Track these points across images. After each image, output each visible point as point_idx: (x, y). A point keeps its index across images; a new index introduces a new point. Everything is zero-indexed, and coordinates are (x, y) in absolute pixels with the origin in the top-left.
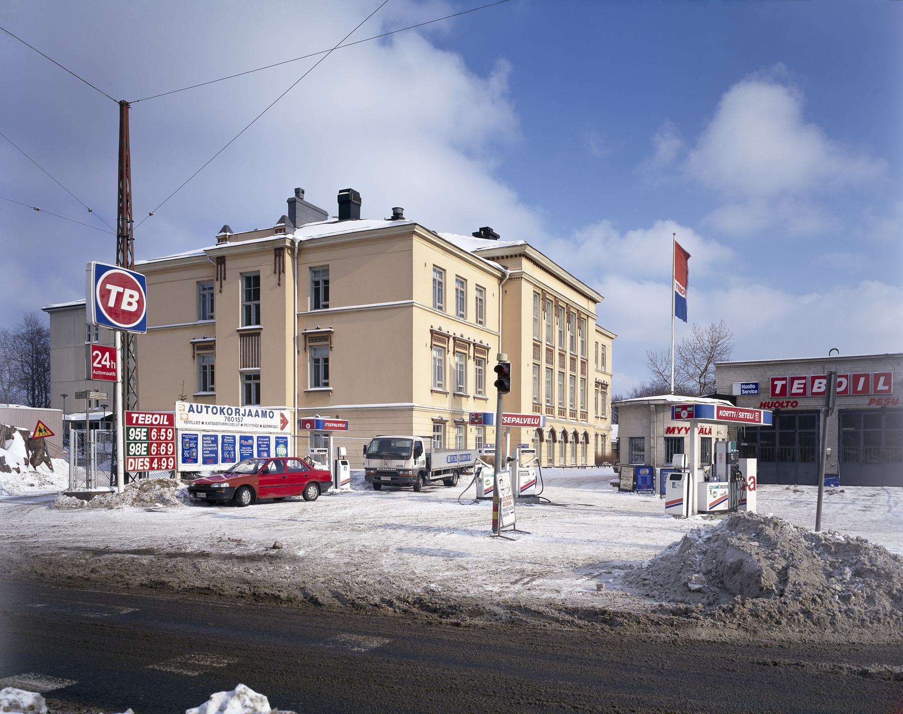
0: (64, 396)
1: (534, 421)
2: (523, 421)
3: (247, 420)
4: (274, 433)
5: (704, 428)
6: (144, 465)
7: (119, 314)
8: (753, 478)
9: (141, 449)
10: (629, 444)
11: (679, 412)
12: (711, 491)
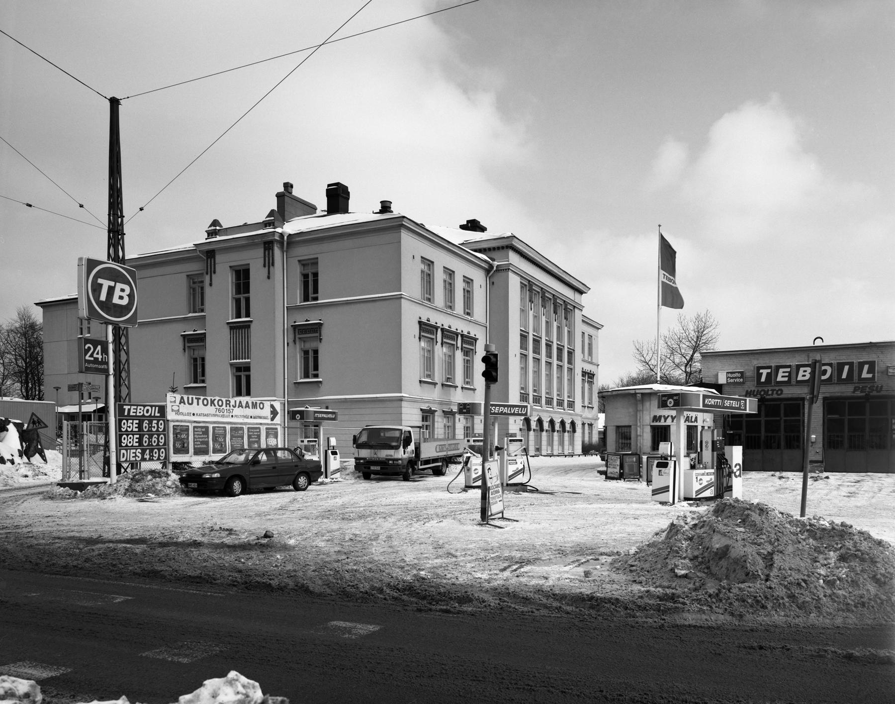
1: (521, 411)
2: (510, 411)
3: (237, 411)
6: (136, 456)
9: (133, 440)
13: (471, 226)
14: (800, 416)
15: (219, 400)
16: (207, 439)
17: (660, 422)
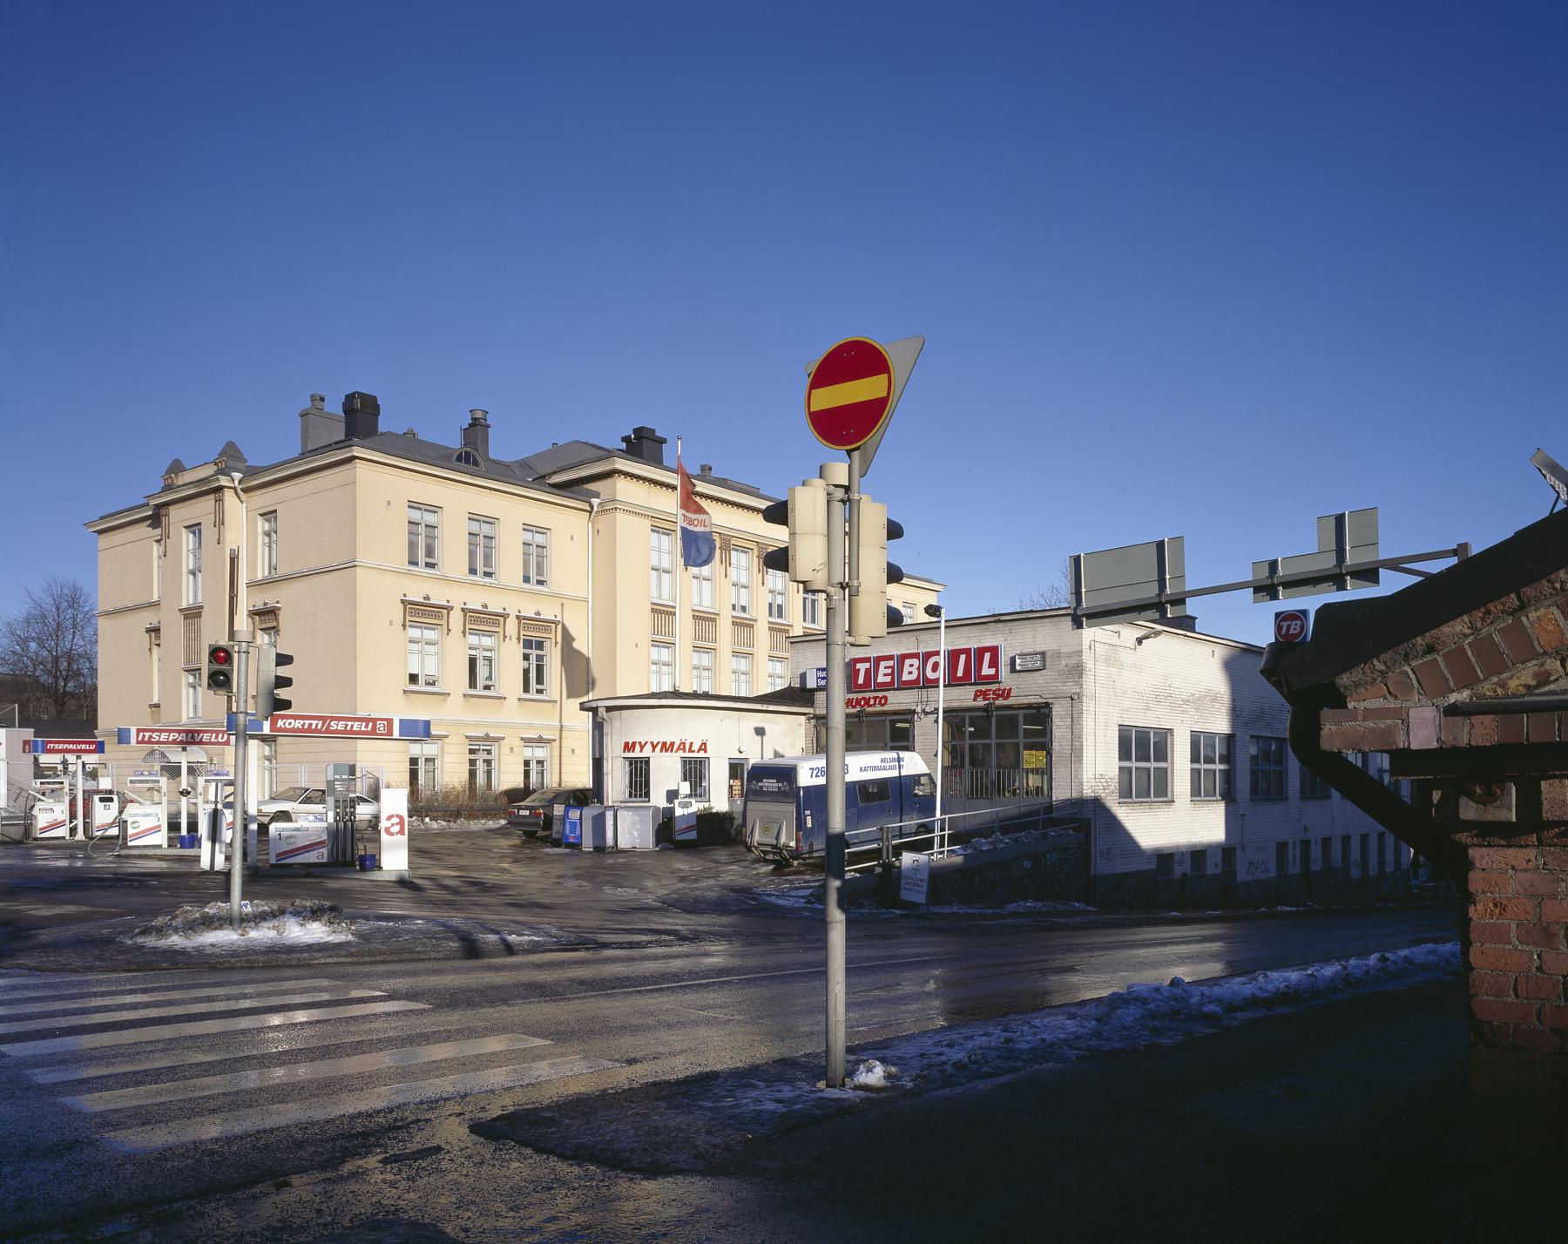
8: (401, 817)
14: (909, 741)
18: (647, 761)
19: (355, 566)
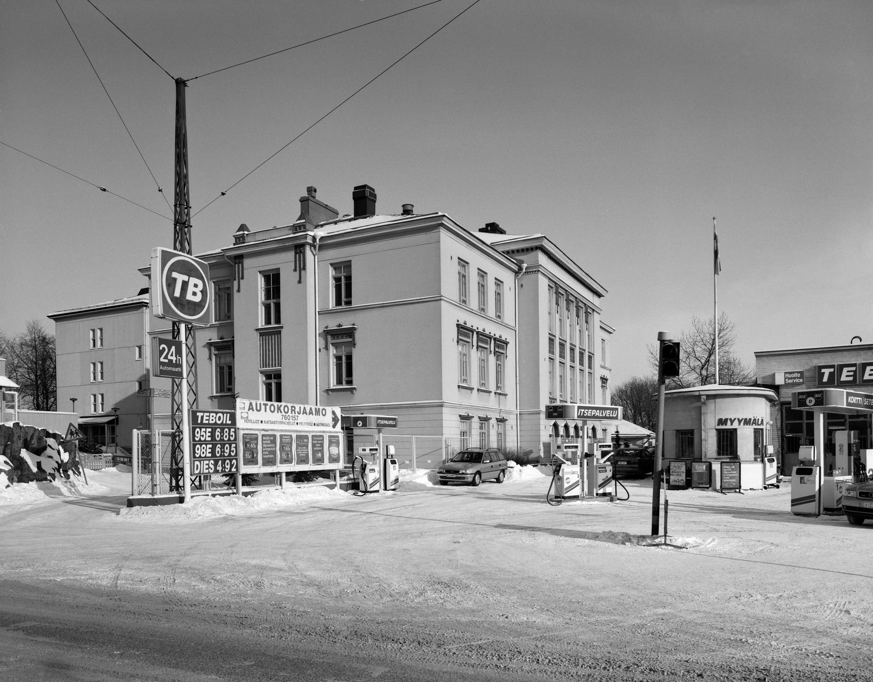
0: (74, 400)
1: (612, 414)
2: (602, 414)
3: (302, 418)
4: (327, 432)
5: (757, 419)
6: (209, 467)
7: (185, 305)
9: (206, 450)
10: (676, 437)
11: (803, 399)
12: (837, 486)
13: (490, 230)
15: (285, 406)
16: (274, 449)
17: (726, 425)
18: (736, 429)
19: (441, 300)
